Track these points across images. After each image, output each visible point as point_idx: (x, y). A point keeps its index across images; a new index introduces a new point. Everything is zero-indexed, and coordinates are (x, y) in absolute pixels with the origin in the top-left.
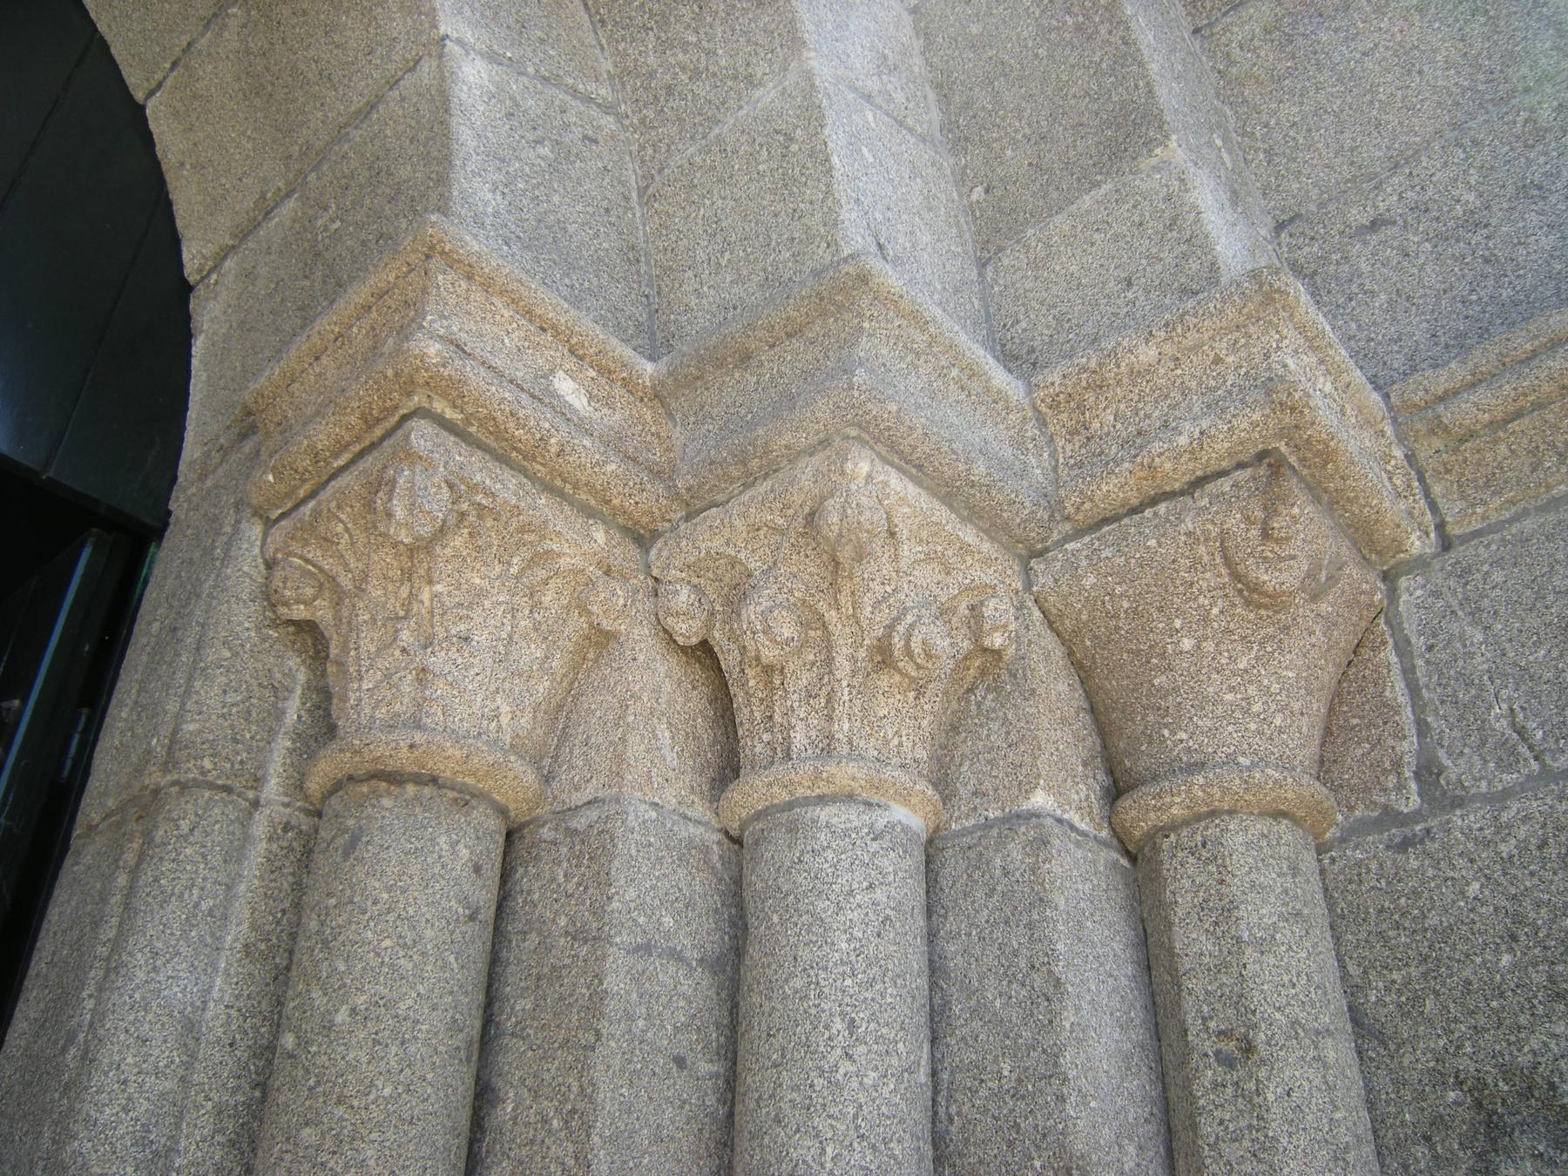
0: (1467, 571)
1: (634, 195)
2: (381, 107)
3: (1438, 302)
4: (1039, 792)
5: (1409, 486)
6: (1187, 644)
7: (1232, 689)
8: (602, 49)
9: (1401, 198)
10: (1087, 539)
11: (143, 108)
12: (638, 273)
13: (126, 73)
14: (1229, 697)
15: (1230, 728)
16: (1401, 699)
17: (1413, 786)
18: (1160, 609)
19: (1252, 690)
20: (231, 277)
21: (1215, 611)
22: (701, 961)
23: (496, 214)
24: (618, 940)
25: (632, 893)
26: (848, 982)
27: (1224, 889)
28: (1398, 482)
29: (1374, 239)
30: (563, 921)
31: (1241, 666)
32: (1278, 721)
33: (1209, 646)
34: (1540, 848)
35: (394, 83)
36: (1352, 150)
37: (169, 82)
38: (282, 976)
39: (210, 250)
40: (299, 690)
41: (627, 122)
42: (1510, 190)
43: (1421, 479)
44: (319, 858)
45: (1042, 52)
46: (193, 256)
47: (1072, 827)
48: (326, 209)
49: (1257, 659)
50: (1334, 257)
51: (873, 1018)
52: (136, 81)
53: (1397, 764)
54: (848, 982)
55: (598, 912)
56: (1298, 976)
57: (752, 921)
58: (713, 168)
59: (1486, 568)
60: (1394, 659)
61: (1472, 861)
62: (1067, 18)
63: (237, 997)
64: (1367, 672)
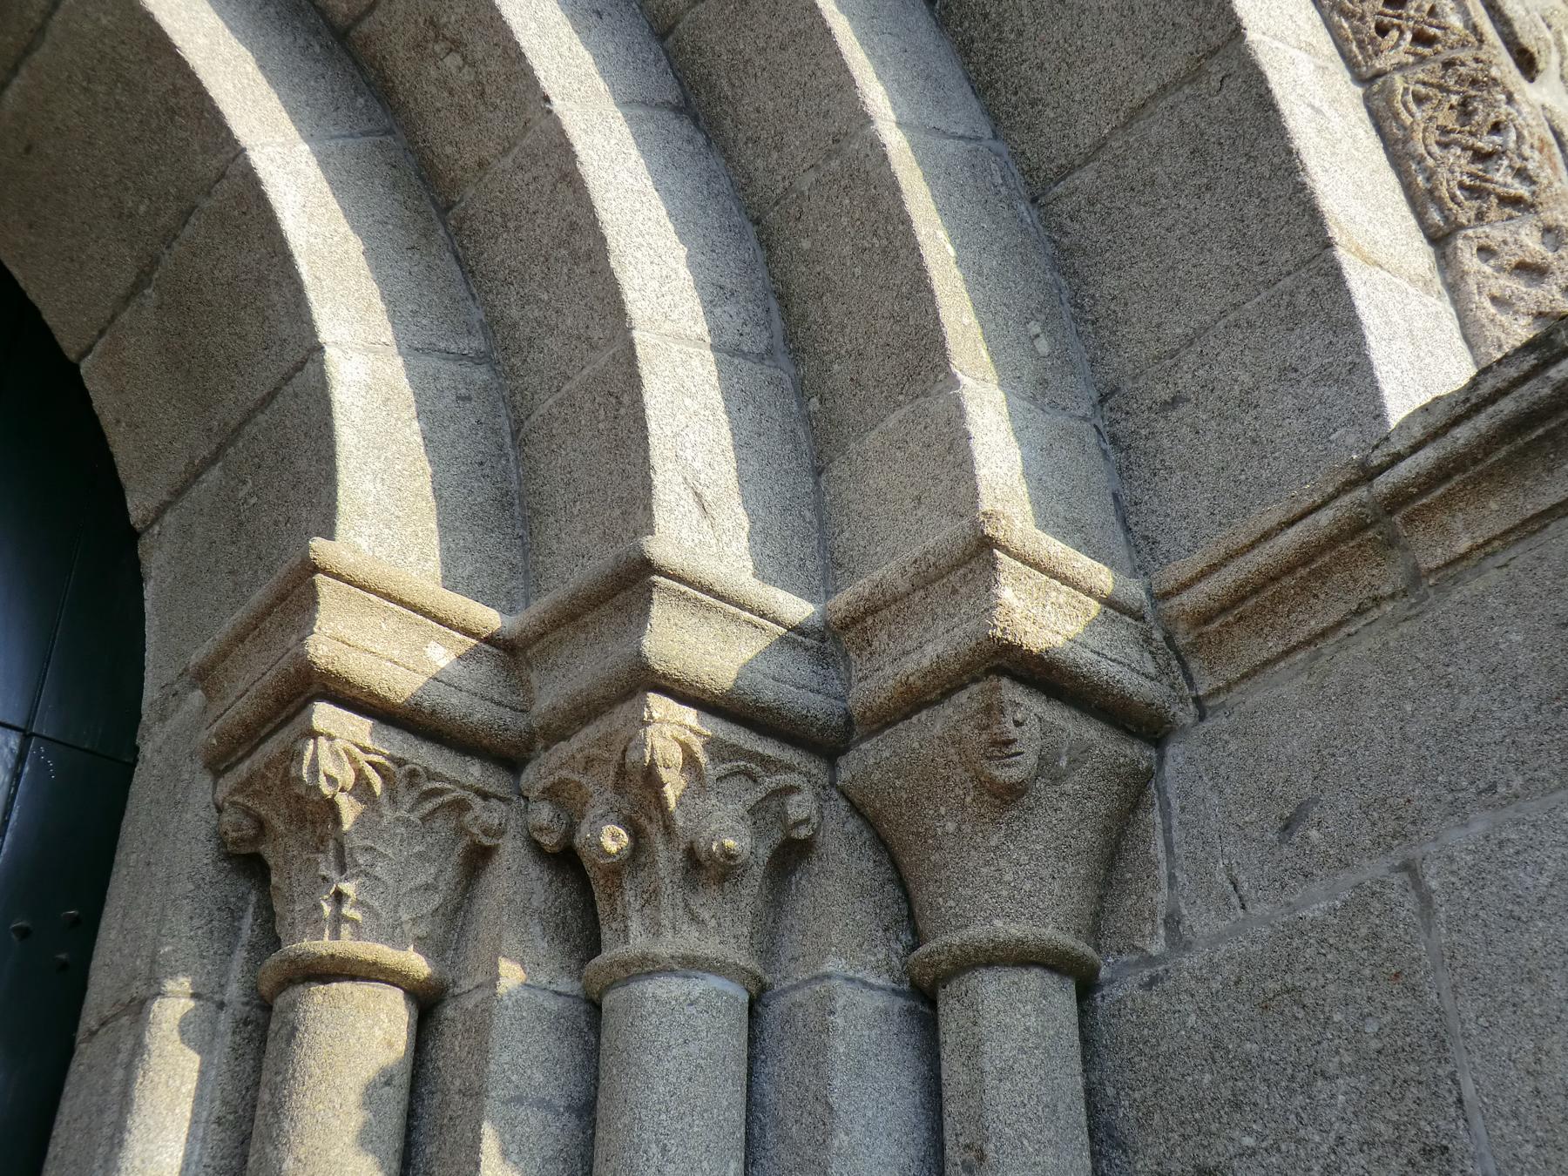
1: (508, 440)
2: (280, 398)
3: (1217, 482)
6: (951, 827)
7: (987, 863)
8: (474, 299)
10: (874, 740)
11: (76, 367)
12: (512, 517)
13: (58, 336)
17: (1161, 932)
18: (928, 798)
19: (1003, 863)
20: (172, 531)
21: (968, 799)
22: (568, 1108)
23: (378, 501)
24: (493, 1094)
25: (506, 1057)
26: (663, 1117)
27: (977, 1030)
29: (1173, 416)
30: (458, 1082)
32: (1027, 886)
33: (967, 828)
34: (1236, 983)
35: (287, 379)
36: (1159, 326)
37: (98, 348)
38: (245, 1140)
39: (151, 504)
40: (251, 910)
41: (498, 368)
42: (1274, 374)
43: (1179, 658)
44: (270, 1046)
45: (858, 271)
46: (137, 506)
47: (865, 984)
48: (245, 482)
50: (1143, 432)
51: (682, 1143)
52: (69, 345)
53: (1153, 913)
54: (663, 1117)
55: (480, 1073)
56: (1030, 1097)
57: (602, 1074)
58: (566, 421)
60: (1159, 820)
62: (875, 240)
63: (213, 1158)
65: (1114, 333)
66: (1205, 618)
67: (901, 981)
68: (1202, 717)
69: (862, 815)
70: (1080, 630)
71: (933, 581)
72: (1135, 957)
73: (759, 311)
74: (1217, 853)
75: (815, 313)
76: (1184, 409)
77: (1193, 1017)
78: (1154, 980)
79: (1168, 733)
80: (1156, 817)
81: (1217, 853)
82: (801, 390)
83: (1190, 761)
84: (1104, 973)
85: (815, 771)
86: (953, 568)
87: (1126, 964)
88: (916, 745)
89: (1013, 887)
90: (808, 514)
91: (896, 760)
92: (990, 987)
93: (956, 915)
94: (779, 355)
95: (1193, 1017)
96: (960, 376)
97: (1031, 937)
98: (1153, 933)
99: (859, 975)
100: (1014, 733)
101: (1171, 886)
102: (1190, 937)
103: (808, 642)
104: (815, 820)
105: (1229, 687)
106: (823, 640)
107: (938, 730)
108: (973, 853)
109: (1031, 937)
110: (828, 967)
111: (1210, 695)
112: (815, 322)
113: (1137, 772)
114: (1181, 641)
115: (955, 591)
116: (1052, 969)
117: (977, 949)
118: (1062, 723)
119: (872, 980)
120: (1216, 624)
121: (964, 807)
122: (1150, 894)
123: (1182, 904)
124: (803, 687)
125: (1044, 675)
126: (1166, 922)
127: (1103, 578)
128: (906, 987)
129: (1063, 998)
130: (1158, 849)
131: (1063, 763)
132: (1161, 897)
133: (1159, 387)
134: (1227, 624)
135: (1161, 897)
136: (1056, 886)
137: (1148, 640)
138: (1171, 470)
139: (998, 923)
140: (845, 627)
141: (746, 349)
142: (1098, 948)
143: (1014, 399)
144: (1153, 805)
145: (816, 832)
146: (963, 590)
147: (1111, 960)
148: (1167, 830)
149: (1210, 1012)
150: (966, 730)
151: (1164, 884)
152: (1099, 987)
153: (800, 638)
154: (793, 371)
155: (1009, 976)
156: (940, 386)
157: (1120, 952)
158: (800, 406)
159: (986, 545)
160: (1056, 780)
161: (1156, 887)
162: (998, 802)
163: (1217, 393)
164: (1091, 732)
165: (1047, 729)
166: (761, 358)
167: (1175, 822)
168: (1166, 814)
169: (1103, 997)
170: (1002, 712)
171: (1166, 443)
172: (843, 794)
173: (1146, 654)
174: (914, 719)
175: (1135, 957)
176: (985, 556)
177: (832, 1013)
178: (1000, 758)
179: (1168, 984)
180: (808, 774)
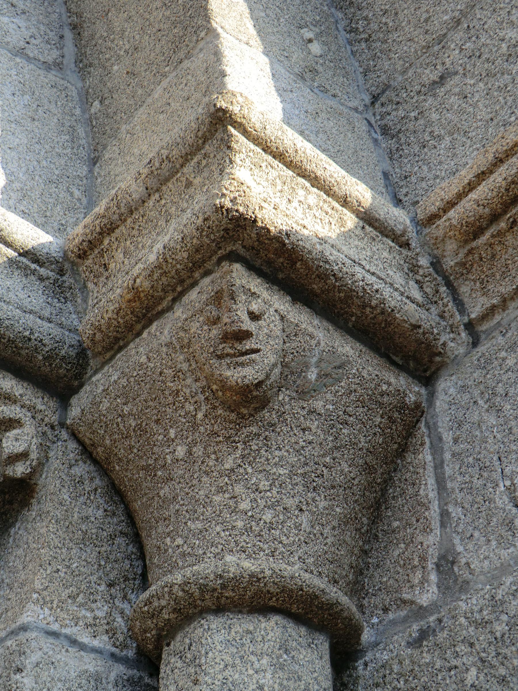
0: (489, 361)
4: (30, 606)
5: (437, 291)
6: (181, 451)
7: (221, 490)
9: (461, 50)
14: (217, 499)
15: (218, 529)
16: (431, 495)
17: (433, 577)
18: (157, 421)
19: (239, 489)
21: (200, 416)
28: (428, 290)
29: (441, 91)
31: (227, 466)
32: (268, 516)
33: (198, 451)
36: (427, 20)
43: (449, 284)
47: (74, 642)
49: (243, 457)
50: (412, 114)
53: (423, 559)
59: (503, 354)
60: (429, 458)
61: (472, 645)
64: (409, 474)
65: (386, 41)
66: (474, 230)
67: (124, 646)
68: (475, 344)
69: (95, 462)
70: (334, 236)
71: (167, 180)
72: (403, 613)
73: (51, 34)
74: (496, 475)
75: (101, 29)
76: (451, 83)
77: (473, 672)
78: (424, 634)
79: (438, 369)
80: (426, 456)
81: (496, 475)
82: (85, 98)
83: (464, 388)
84: (367, 636)
85: (40, 407)
86: (186, 158)
87: (393, 623)
88: (143, 359)
89: (253, 514)
90: (77, 193)
91: (124, 382)
92: (217, 638)
93: (184, 555)
94: (68, 72)
95: (473, 672)
96: (220, 30)
97: (268, 573)
98: (424, 580)
99: (67, 631)
100: (248, 325)
101: (443, 525)
102: (467, 576)
103: (43, 271)
104: (34, 456)
105: (504, 303)
106: (61, 272)
107: (165, 337)
108: (205, 479)
109: (268, 573)
110: (25, 618)
111: (484, 317)
112: (102, 36)
113: (402, 407)
114: (449, 262)
115: (189, 184)
116: (298, 619)
117: (203, 589)
118: (311, 329)
119: (85, 639)
120: (488, 235)
121: (195, 426)
122: (420, 538)
123: (457, 541)
124: (31, 312)
125: (281, 262)
126: (438, 566)
127: (363, 193)
128: (131, 653)
129: (313, 659)
130: (429, 488)
131: (312, 375)
132: (432, 541)
133: (427, 71)
134: (500, 234)
135: (432, 541)
136: (304, 519)
137: (414, 269)
138: (440, 138)
139: (229, 558)
140: (83, 255)
141: (31, 55)
142: (361, 607)
143: (277, 66)
144: (422, 444)
145: (35, 471)
146: (197, 181)
147: (375, 620)
148: (439, 466)
149: (495, 662)
150: (194, 327)
151: (436, 524)
152: (362, 652)
153: (33, 266)
154: (80, 85)
155: (241, 625)
156: (201, 44)
157: (386, 610)
158: (84, 112)
159: (220, 121)
160: (303, 394)
161: (427, 530)
162: (233, 416)
163: (484, 57)
164: (347, 348)
165: (291, 333)
166: (47, 66)
167: (447, 456)
168: (437, 449)
169: (366, 664)
170: (233, 297)
171: (435, 116)
172: (74, 435)
173: (412, 283)
174: (145, 335)
175: (403, 613)
176: (219, 135)
177: (19, 670)
178: (234, 355)
179: (442, 636)
180: (31, 408)
